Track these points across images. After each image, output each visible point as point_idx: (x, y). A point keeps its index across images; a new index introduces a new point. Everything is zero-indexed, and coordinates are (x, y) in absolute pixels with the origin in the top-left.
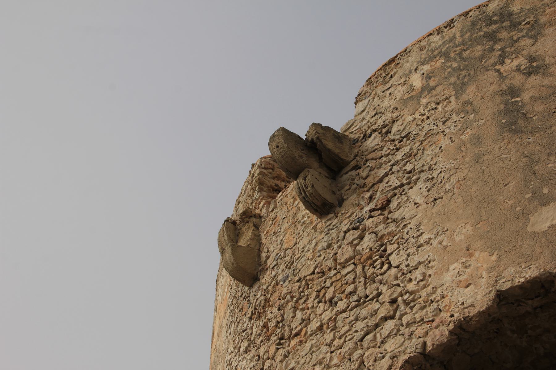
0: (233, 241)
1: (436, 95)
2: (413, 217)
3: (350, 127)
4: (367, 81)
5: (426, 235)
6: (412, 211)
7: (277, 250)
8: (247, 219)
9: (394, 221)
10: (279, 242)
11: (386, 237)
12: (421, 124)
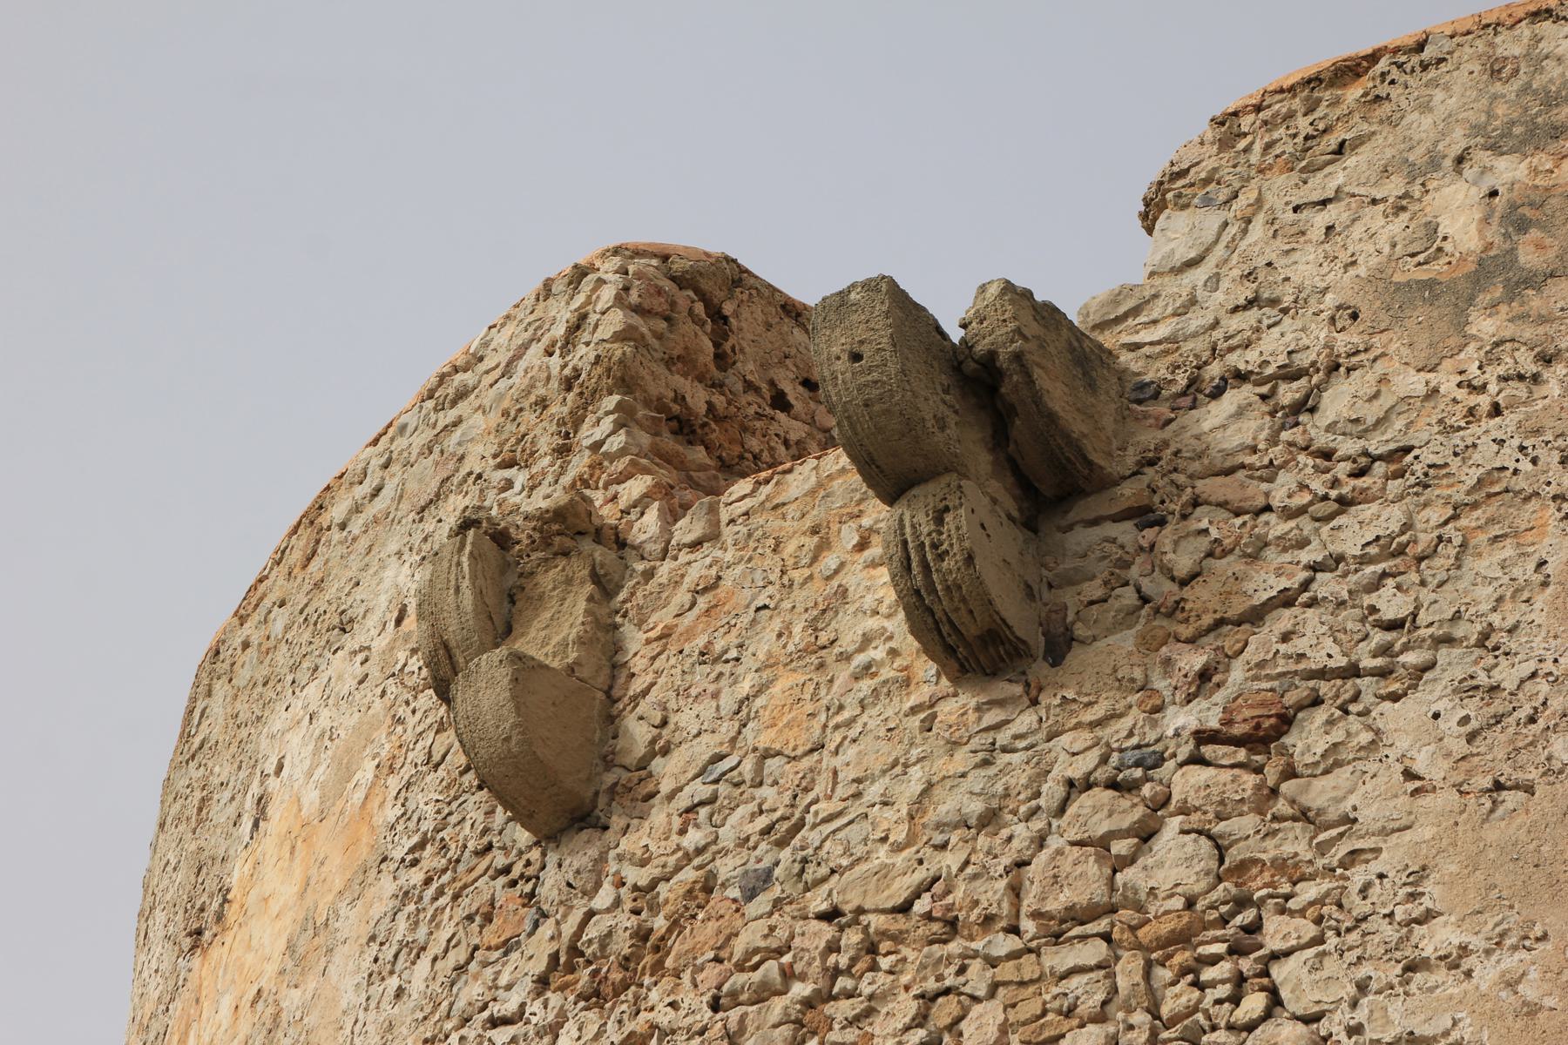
0: (491, 618)
1: (1543, 320)
2: (1394, 831)
3: (1126, 316)
4: (1219, 122)
5: (1449, 928)
6: (1391, 804)
7: (717, 738)
8: (565, 539)
9: (1304, 815)
10: (727, 702)
11: (1262, 872)
12: (1460, 429)
